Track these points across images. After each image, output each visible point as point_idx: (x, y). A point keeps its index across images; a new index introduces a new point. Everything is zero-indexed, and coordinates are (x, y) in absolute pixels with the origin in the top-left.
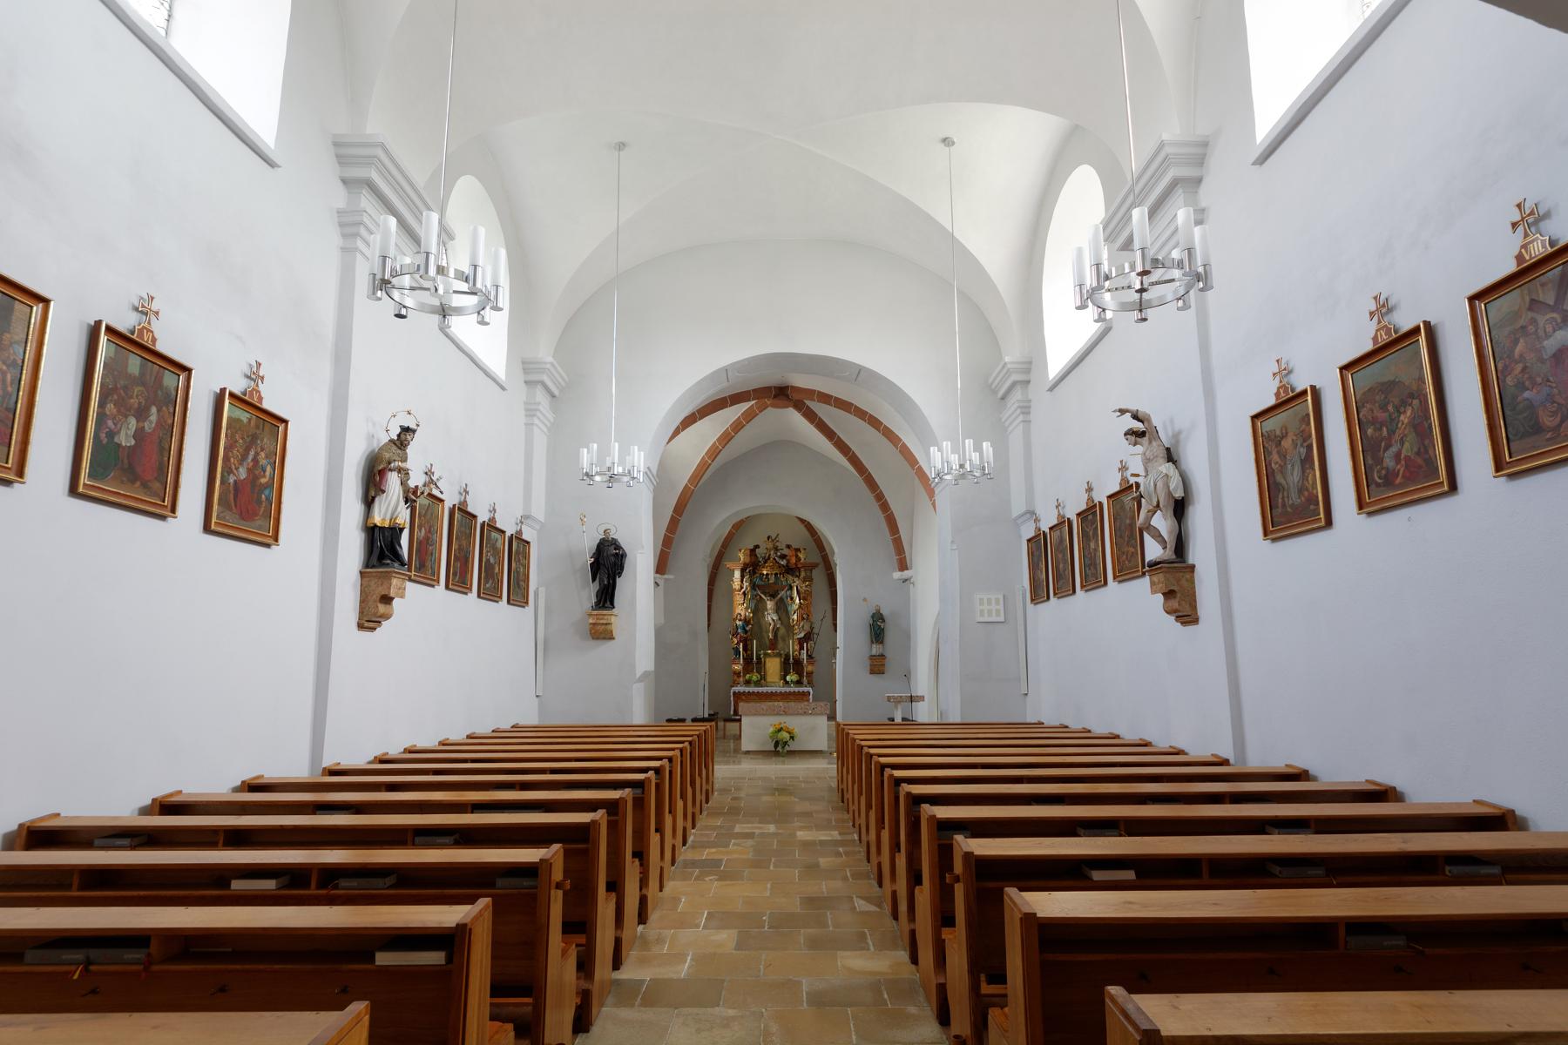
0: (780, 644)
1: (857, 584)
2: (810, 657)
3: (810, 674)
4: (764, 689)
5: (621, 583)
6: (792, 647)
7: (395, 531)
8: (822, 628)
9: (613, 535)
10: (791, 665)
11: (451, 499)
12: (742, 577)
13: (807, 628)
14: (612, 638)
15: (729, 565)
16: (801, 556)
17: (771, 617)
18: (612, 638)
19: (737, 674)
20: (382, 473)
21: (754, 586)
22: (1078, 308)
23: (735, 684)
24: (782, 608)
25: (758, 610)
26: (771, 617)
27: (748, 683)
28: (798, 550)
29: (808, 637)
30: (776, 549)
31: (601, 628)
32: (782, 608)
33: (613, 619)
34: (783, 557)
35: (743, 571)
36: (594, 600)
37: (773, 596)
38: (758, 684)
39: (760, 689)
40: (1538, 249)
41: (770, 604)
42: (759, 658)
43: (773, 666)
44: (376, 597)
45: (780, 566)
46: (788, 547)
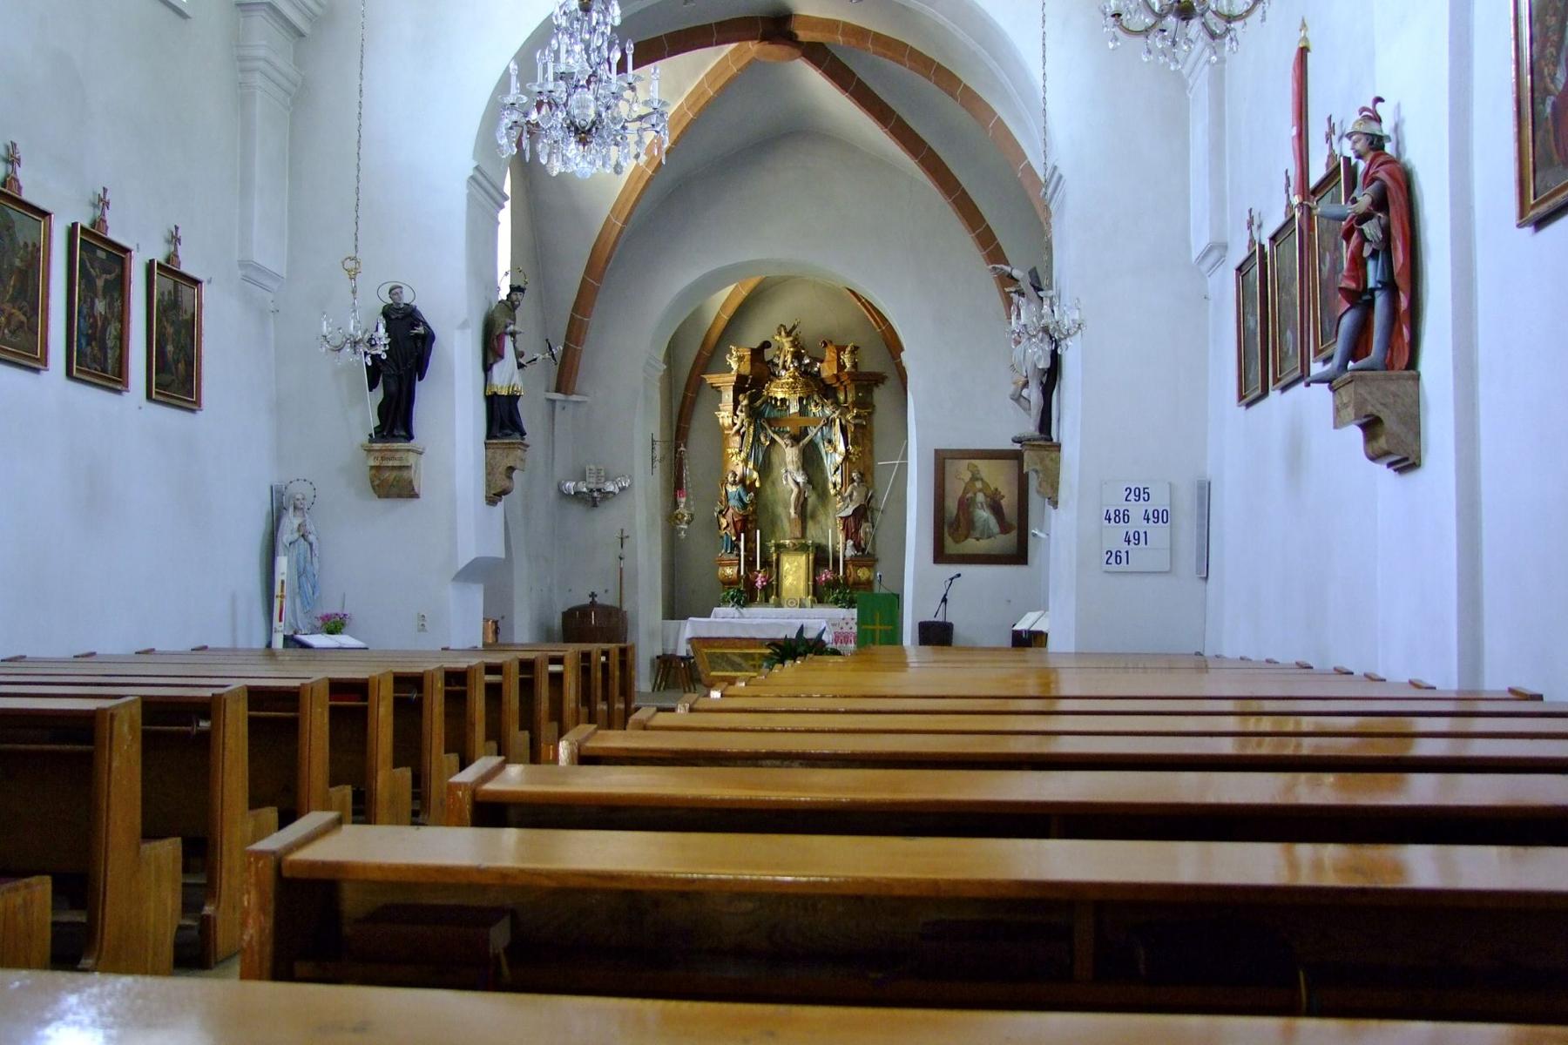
1: (951, 402)
5: (421, 388)
7: (513, 399)
9: (407, 298)
11: (68, 212)
12: (736, 403)
14: (413, 495)
15: (712, 379)
18: (413, 495)
20: (500, 338)
31: (389, 476)
32: (811, 460)
33: (411, 459)
35: (738, 389)
36: (374, 421)
44: (502, 469)
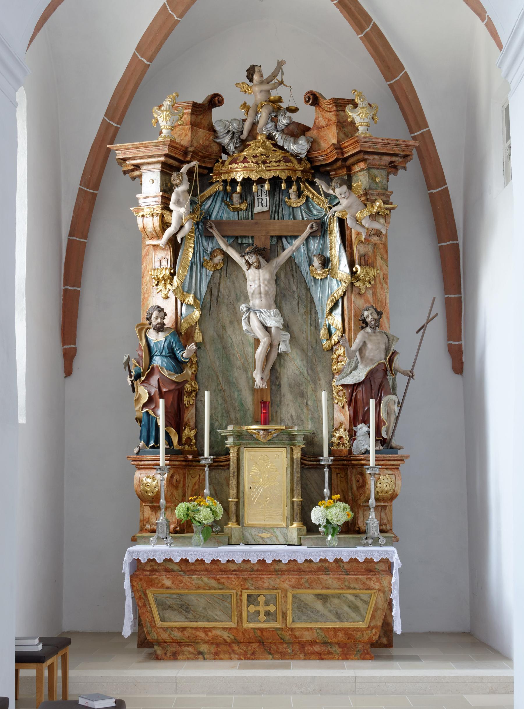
0: (289, 408)
2: (384, 443)
3: (385, 500)
4: (237, 553)
6: (330, 416)
8: (422, 353)
10: (328, 473)
12: (167, 190)
13: (376, 353)
16: (357, 117)
17: (258, 317)
19: (151, 501)
21: (204, 226)
22: (406, 170)
23: (146, 531)
24: (292, 290)
25: (218, 298)
26: (258, 317)
27: (183, 528)
28: (340, 104)
29: (379, 382)
30: (275, 106)
34: (298, 131)
35: (168, 169)
37: (265, 254)
38: (215, 532)
39: (223, 553)
40: (274, 305)
41: (256, 280)
42: (220, 453)
43: (266, 473)
45: (288, 157)
46: (314, 99)
